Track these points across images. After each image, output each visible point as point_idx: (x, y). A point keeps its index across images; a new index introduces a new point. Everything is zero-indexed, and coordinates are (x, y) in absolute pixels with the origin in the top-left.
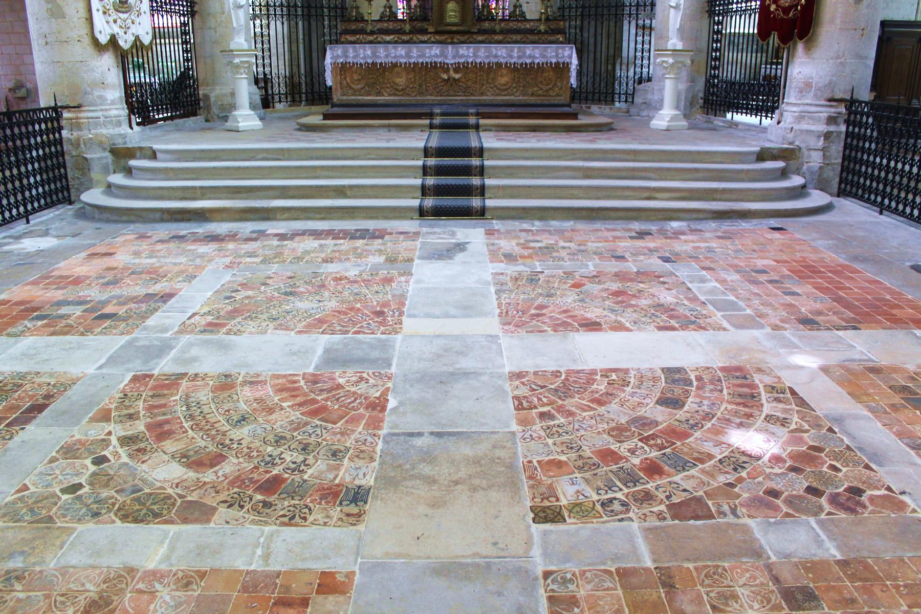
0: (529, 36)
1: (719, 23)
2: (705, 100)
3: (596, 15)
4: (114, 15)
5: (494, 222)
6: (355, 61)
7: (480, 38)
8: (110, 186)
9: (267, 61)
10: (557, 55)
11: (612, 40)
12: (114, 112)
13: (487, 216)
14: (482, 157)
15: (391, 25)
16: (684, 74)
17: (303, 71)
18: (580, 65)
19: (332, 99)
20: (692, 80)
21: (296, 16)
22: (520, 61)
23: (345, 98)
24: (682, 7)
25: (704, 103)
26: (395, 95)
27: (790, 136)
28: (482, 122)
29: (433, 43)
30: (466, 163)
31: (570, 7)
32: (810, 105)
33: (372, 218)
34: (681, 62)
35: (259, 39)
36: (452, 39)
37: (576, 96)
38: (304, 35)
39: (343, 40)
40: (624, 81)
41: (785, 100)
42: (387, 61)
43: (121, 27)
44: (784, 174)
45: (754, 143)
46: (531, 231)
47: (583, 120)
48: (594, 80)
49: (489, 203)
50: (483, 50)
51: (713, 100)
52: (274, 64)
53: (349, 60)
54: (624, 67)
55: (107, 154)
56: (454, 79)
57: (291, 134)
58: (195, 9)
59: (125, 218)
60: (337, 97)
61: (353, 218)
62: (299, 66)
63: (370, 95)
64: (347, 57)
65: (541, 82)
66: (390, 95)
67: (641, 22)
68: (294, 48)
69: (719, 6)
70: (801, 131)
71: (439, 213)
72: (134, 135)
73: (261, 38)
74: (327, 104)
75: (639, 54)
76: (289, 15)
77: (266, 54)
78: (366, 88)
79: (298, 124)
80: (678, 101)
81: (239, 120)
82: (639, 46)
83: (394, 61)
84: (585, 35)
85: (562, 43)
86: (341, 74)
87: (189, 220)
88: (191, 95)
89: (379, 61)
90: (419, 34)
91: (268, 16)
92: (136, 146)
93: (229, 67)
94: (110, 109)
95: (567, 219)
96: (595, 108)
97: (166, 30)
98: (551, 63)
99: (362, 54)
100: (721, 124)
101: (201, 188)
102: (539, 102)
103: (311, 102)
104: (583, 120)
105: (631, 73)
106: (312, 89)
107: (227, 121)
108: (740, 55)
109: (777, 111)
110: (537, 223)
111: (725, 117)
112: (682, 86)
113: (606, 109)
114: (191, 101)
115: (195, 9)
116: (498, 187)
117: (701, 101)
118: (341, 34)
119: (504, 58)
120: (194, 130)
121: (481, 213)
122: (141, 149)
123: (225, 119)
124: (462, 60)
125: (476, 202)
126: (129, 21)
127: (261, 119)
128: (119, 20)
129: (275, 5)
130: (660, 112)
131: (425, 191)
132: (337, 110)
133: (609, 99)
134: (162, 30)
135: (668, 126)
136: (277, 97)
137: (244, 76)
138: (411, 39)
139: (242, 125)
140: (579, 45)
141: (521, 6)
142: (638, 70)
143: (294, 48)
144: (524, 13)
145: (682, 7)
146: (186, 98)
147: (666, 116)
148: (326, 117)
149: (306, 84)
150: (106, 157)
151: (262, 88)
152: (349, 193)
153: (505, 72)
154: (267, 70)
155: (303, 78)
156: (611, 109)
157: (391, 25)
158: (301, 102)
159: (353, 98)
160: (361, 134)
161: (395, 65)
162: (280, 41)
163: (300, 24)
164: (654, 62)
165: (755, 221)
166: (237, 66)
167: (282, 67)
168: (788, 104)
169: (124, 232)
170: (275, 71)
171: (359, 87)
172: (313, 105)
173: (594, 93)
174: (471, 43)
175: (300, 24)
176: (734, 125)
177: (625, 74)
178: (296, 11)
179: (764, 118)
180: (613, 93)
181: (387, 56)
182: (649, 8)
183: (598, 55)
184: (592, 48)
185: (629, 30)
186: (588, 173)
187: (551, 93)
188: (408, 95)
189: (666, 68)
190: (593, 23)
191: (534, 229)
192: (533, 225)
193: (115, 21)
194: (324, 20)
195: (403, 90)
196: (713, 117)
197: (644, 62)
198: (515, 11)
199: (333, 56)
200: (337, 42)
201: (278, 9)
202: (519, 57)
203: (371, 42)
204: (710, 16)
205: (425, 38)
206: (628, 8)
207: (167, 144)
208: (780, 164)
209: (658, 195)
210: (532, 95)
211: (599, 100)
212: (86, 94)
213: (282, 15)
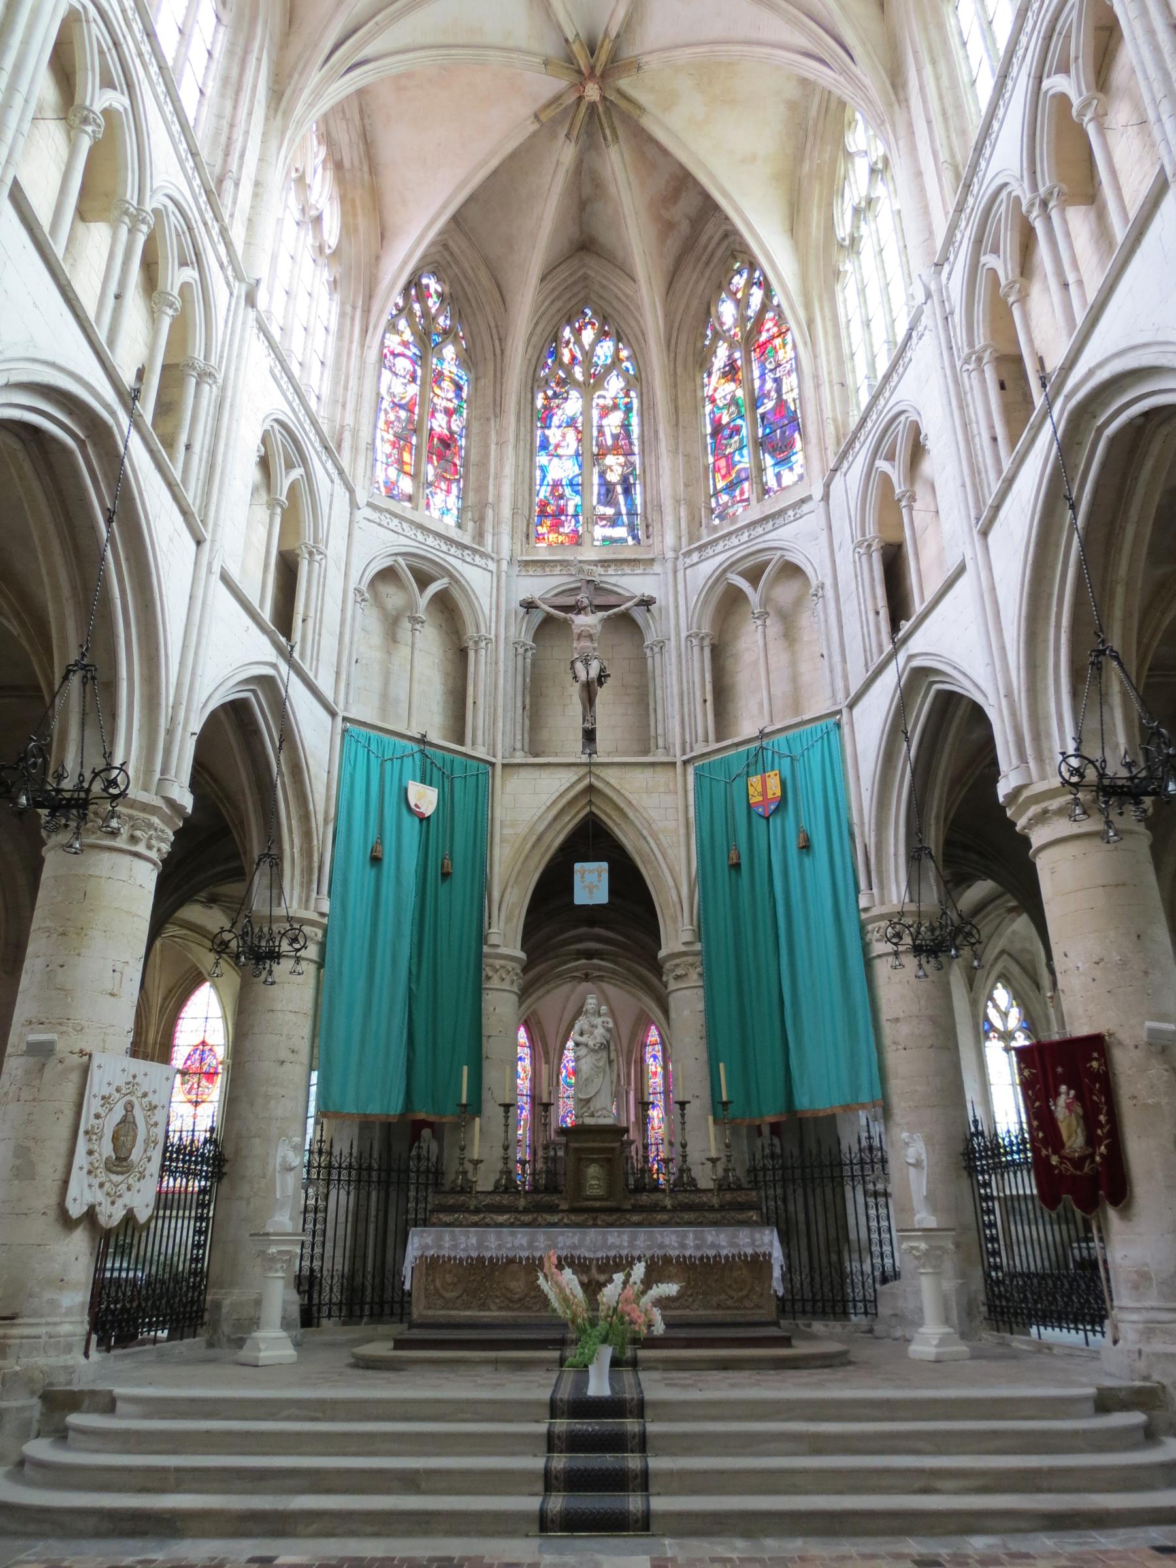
0: (707, 1214)
1: (987, 1185)
2: (989, 1307)
3: (803, 1179)
4: (102, 1176)
5: (667, 1541)
6: (453, 1254)
7: (636, 1218)
8: (22, 1463)
9: (318, 1250)
10: (753, 1241)
11: (831, 1215)
12: (66, 1328)
13: (654, 1527)
14: (642, 1417)
15: (506, 1200)
16: (948, 1265)
17: (370, 1268)
18: (788, 1256)
19: (410, 1314)
20: (963, 1274)
21: (369, 1182)
22: (699, 1254)
23: (430, 1313)
24: (925, 1163)
25: (990, 1311)
26: (508, 1308)
27: (1141, 1365)
28: (642, 1353)
29: (567, 1226)
30: (616, 1428)
31: (764, 1169)
32: (1159, 1309)
33: (460, 1534)
34: (939, 1248)
35: (310, 1216)
36: (595, 1219)
37: (786, 1306)
38: (378, 1210)
39: (434, 1220)
40: (858, 1279)
41: (1115, 1303)
42: (500, 1254)
43: (108, 1194)
44: (1149, 1435)
45: (1084, 1380)
46: (730, 1560)
47: (801, 1348)
48: (812, 1279)
49: (659, 1504)
50: (642, 1237)
51: (1002, 1307)
52: (328, 1253)
53: (441, 1253)
54: (855, 1256)
55: (35, 1401)
56: (598, 1282)
57: (340, 1374)
58: (225, 1170)
59: (32, 1527)
60: (418, 1310)
61: (426, 1533)
62: (365, 1257)
63: (469, 1308)
64: (440, 1247)
65: (729, 1286)
66: (500, 1309)
67: (870, 1187)
68: (361, 1230)
69: (981, 1158)
70: (1157, 1355)
71: (574, 1524)
72: (89, 1368)
73: (313, 1213)
74: (401, 1322)
75: (875, 1236)
76: (359, 1181)
77: (318, 1239)
78: (464, 1297)
79: (354, 1356)
80: (946, 1308)
81: (262, 1346)
82: (874, 1224)
83: (511, 1254)
84: (791, 1208)
85: (756, 1224)
86: (427, 1275)
87: (143, 1534)
88: (192, 1302)
89: (487, 1254)
90: (546, 1212)
91: (328, 1182)
92: (86, 1388)
93: (259, 1259)
94: (61, 1323)
95: (793, 1533)
96: (818, 1327)
97: (176, 1196)
98: (746, 1255)
99: (463, 1242)
100: (1024, 1347)
101: (178, 1470)
102: (729, 1320)
103: (377, 1317)
104: (801, 1348)
105: (867, 1268)
106: (381, 1297)
107: (241, 1347)
108: (1034, 1228)
109: (1107, 1322)
110: (740, 1543)
111: (1029, 1334)
112: (949, 1285)
113: (837, 1327)
114: (191, 1313)
115: (225, 1170)
116: (671, 1473)
117: (984, 1309)
118: (432, 1212)
119: (674, 1248)
120: (187, 1362)
121: (643, 1524)
122: (93, 1393)
123: (239, 1343)
124: (612, 1253)
125: (634, 1503)
126: (124, 1186)
127: (297, 1345)
128: (107, 1185)
129: (340, 1167)
130: (922, 1330)
131: (550, 1482)
132: (417, 1334)
133: (839, 1309)
134: (170, 1196)
135: (938, 1354)
136: (325, 1309)
137: (280, 1274)
138: (535, 1219)
139: (267, 1354)
140: (783, 1226)
141: (689, 1170)
142: (877, 1261)
143: (361, 1230)
144: (694, 1179)
145: (925, 1163)
146: (185, 1306)
147: (930, 1338)
148: (400, 1344)
149: (373, 1289)
150: (32, 1407)
151: (304, 1292)
152: (423, 1485)
153: (673, 1270)
154: (317, 1264)
155: (369, 1277)
156: (844, 1327)
157: (506, 1200)
158: (361, 1317)
159: (443, 1312)
160: (452, 1376)
161: (511, 1261)
162: (342, 1219)
163: (374, 1195)
164: (899, 1248)
165: (1122, 1533)
166: (272, 1259)
167: (339, 1259)
168: (1121, 1308)
169: (22, 1557)
170: (327, 1265)
171: (454, 1294)
172: (380, 1322)
173: (814, 1301)
174: (622, 1226)
175: (374, 1195)
176: (1045, 1348)
177: (860, 1267)
178: (370, 1176)
179: (1090, 1334)
180: (844, 1301)
181: (499, 1247)
182: (878, 1166)
183: (814, 1238)
184: (802, 1227)
185: (855, 1199)
186: (819, 1445)
187: (747, 1303)
188: (528, 1309)
189: (917, 1258)
190: (800, 1191)
191: (734, 1556)
192: (735, 1549)
193: (101, 1185)
194: (408, 1190)
195: (520, 1300)
196: (1008, 1335)
197: (885, 1248)
198: (681, 1177)
199: (420, 1244)
200: (425, 1223)
201: (344, 1172)
202: (698, 1247)
203: (475, 1225)
204: (970, 1175)
205: (555, 1218)
206: (848, 1168)
207: (139, 1385)
208: (1137, 1418)
209: (939, 1484)
210: (719, 1307)
211: (824, 1313)
212: (30, 1296)
213: (349, 1181)
